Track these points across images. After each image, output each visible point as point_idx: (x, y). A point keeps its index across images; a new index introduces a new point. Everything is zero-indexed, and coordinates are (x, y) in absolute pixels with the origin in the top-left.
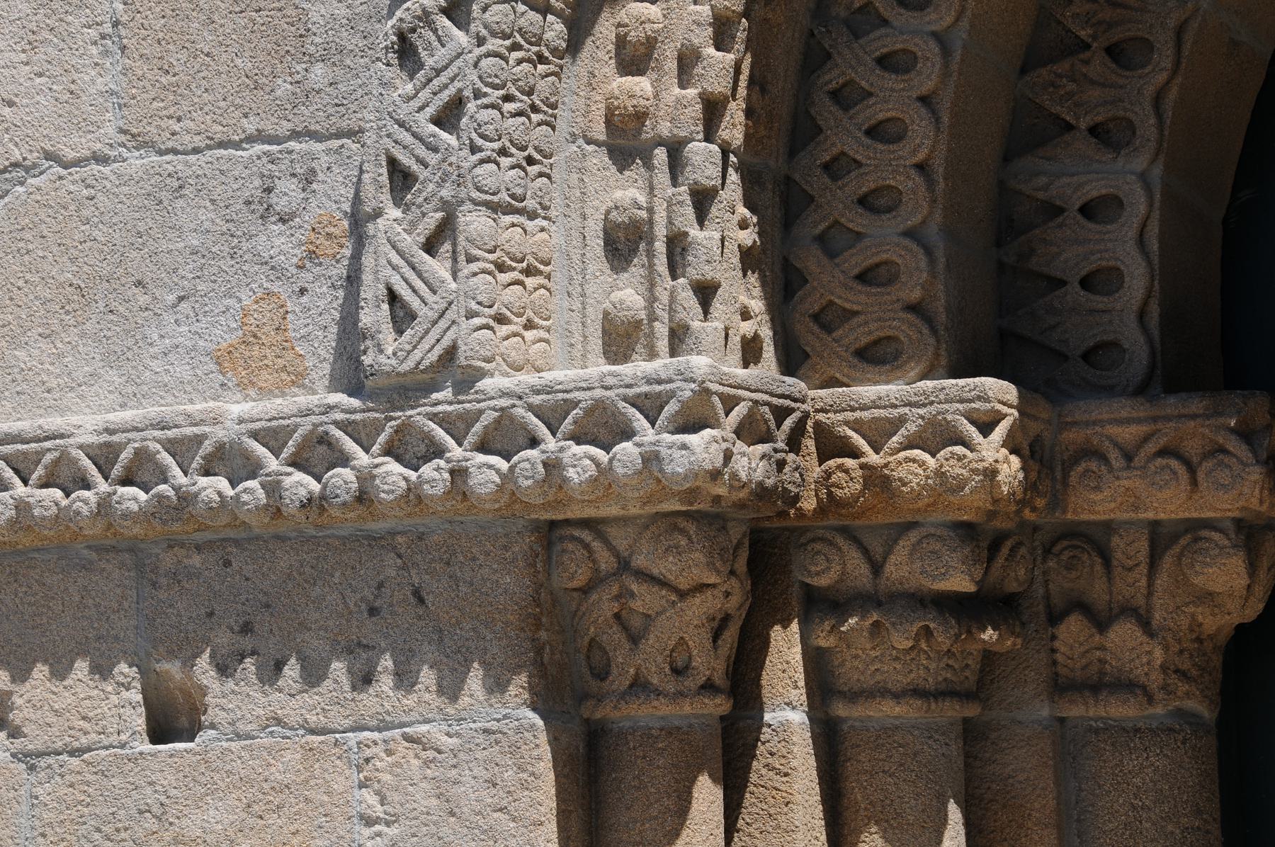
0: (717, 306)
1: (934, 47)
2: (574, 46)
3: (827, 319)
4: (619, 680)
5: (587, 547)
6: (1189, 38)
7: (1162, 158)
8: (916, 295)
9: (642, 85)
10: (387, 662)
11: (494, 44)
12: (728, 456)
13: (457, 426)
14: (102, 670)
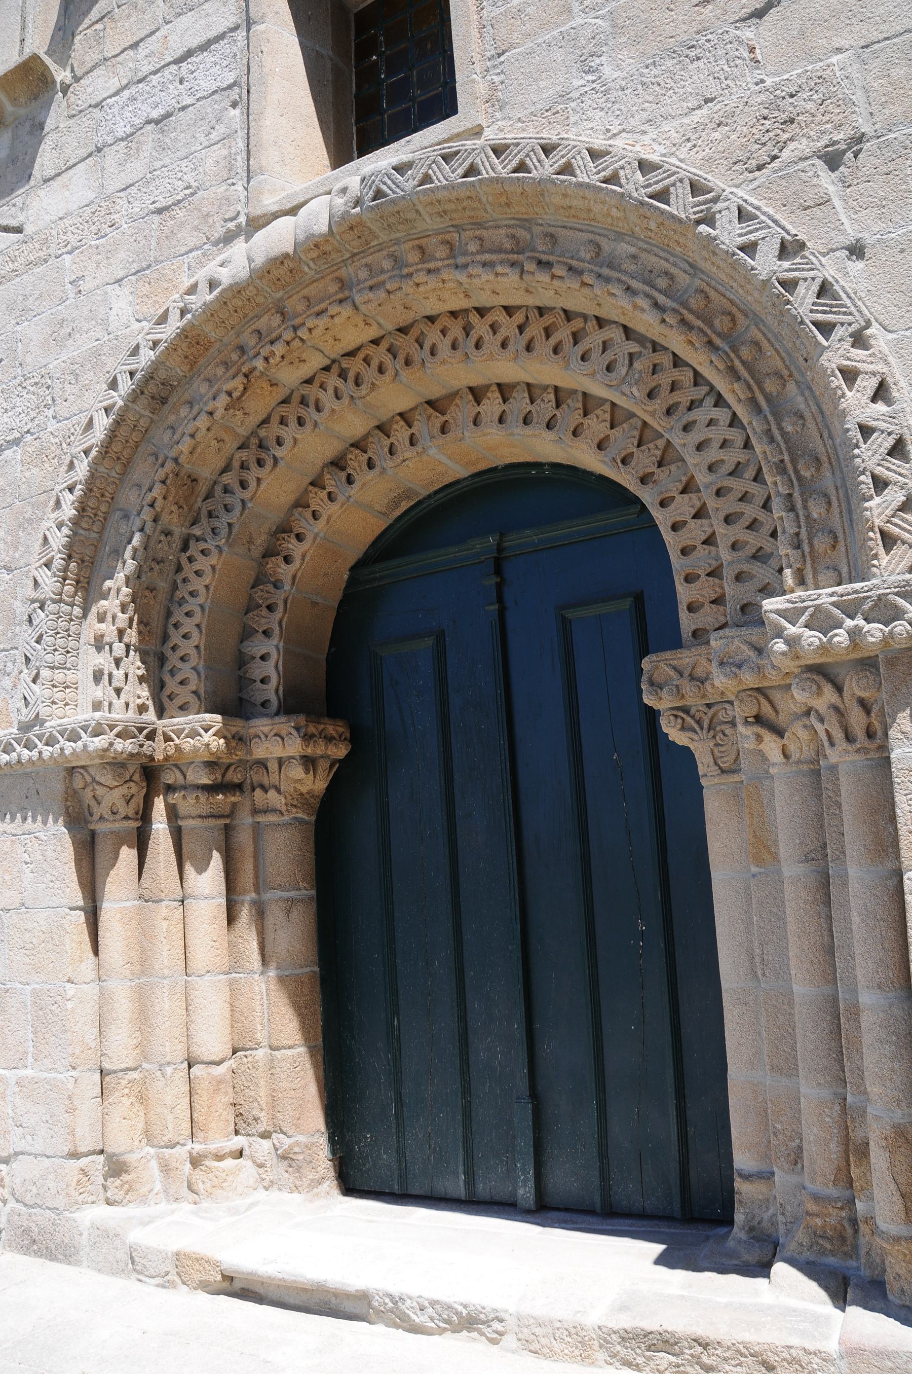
0: (122, 695)
1: (199, 608)
2: (85, 616)
4: (96, 817)
5: (82, 774)
6: (289, 602)
8: (194, 688)
10: (30, 814)
11: (51, 617)
12: (111, 744)
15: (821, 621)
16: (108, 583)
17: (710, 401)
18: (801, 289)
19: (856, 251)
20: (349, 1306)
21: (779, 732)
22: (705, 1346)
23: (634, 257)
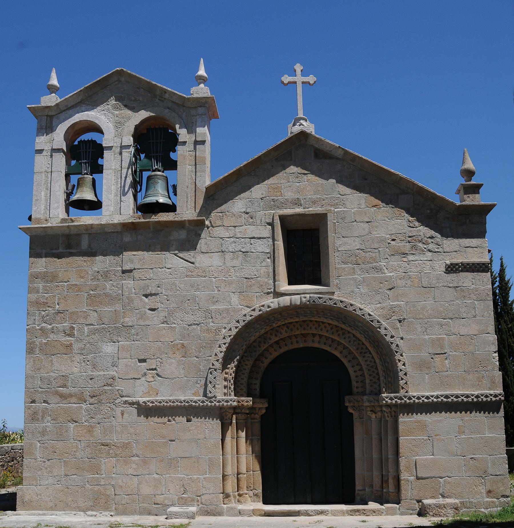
3: (238, 392)
7: (232, 367)
9: (227, 376)
13: (215, 401)
14: (183, 417)
15: (391, 399)
16: (229, 366)
17: (368, 353)
18: (393, 344)
19: (402, 338)
20: (293, 514)
21: (375, 413)
22: (364, 510)
23: (362, 327)
